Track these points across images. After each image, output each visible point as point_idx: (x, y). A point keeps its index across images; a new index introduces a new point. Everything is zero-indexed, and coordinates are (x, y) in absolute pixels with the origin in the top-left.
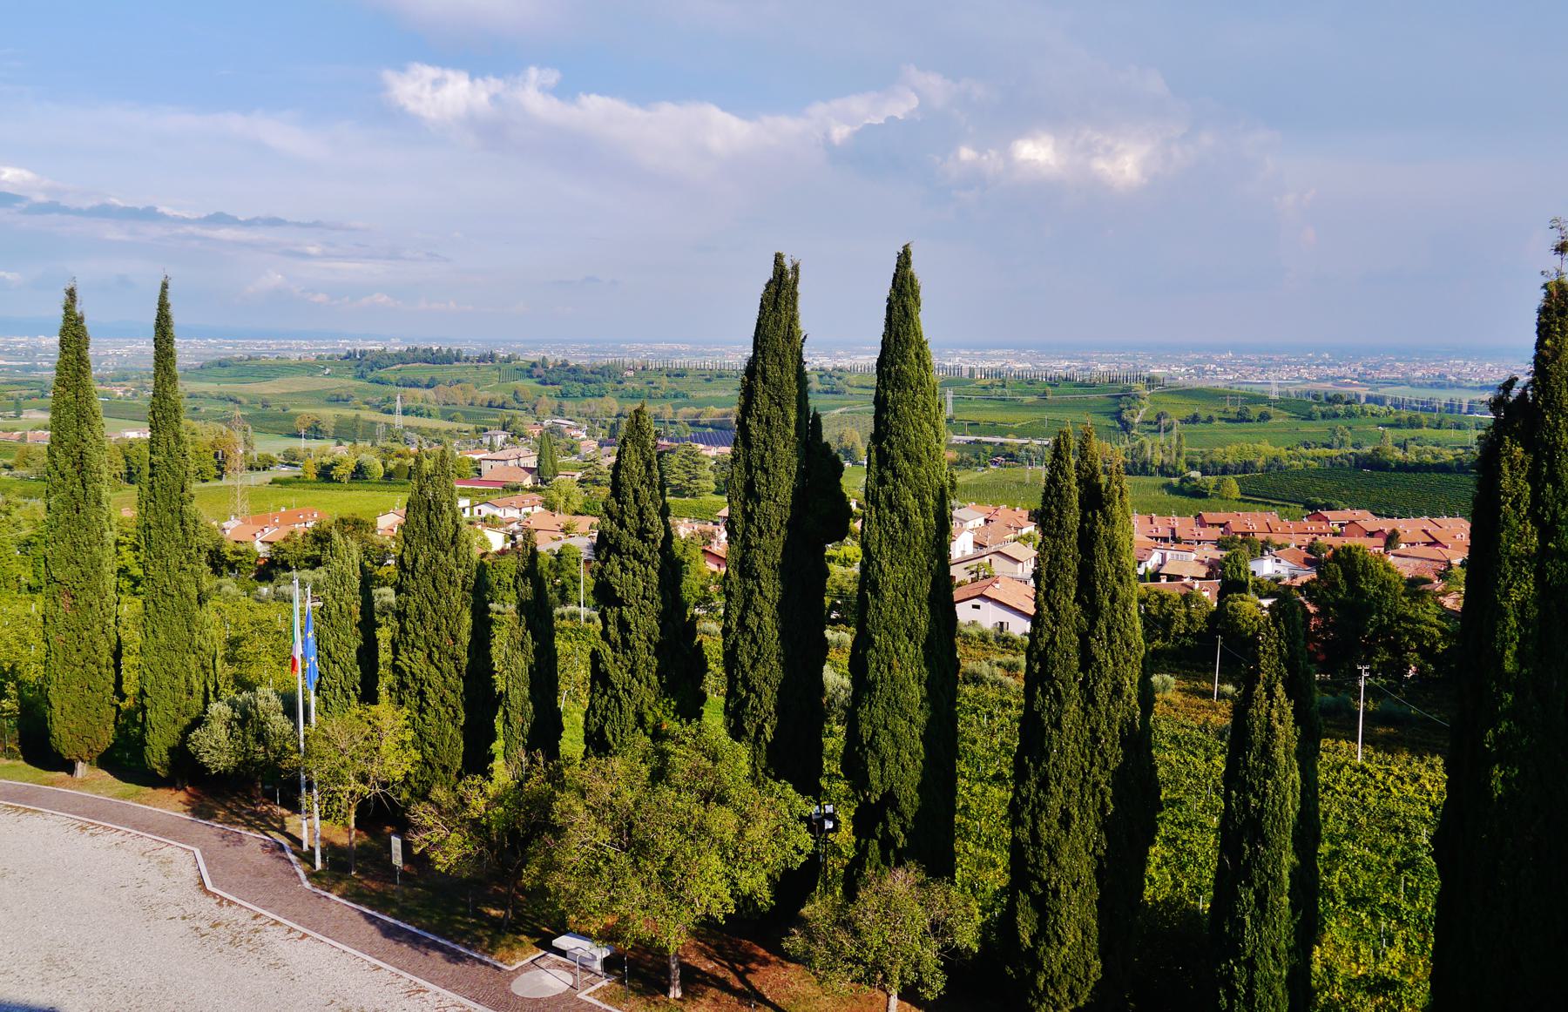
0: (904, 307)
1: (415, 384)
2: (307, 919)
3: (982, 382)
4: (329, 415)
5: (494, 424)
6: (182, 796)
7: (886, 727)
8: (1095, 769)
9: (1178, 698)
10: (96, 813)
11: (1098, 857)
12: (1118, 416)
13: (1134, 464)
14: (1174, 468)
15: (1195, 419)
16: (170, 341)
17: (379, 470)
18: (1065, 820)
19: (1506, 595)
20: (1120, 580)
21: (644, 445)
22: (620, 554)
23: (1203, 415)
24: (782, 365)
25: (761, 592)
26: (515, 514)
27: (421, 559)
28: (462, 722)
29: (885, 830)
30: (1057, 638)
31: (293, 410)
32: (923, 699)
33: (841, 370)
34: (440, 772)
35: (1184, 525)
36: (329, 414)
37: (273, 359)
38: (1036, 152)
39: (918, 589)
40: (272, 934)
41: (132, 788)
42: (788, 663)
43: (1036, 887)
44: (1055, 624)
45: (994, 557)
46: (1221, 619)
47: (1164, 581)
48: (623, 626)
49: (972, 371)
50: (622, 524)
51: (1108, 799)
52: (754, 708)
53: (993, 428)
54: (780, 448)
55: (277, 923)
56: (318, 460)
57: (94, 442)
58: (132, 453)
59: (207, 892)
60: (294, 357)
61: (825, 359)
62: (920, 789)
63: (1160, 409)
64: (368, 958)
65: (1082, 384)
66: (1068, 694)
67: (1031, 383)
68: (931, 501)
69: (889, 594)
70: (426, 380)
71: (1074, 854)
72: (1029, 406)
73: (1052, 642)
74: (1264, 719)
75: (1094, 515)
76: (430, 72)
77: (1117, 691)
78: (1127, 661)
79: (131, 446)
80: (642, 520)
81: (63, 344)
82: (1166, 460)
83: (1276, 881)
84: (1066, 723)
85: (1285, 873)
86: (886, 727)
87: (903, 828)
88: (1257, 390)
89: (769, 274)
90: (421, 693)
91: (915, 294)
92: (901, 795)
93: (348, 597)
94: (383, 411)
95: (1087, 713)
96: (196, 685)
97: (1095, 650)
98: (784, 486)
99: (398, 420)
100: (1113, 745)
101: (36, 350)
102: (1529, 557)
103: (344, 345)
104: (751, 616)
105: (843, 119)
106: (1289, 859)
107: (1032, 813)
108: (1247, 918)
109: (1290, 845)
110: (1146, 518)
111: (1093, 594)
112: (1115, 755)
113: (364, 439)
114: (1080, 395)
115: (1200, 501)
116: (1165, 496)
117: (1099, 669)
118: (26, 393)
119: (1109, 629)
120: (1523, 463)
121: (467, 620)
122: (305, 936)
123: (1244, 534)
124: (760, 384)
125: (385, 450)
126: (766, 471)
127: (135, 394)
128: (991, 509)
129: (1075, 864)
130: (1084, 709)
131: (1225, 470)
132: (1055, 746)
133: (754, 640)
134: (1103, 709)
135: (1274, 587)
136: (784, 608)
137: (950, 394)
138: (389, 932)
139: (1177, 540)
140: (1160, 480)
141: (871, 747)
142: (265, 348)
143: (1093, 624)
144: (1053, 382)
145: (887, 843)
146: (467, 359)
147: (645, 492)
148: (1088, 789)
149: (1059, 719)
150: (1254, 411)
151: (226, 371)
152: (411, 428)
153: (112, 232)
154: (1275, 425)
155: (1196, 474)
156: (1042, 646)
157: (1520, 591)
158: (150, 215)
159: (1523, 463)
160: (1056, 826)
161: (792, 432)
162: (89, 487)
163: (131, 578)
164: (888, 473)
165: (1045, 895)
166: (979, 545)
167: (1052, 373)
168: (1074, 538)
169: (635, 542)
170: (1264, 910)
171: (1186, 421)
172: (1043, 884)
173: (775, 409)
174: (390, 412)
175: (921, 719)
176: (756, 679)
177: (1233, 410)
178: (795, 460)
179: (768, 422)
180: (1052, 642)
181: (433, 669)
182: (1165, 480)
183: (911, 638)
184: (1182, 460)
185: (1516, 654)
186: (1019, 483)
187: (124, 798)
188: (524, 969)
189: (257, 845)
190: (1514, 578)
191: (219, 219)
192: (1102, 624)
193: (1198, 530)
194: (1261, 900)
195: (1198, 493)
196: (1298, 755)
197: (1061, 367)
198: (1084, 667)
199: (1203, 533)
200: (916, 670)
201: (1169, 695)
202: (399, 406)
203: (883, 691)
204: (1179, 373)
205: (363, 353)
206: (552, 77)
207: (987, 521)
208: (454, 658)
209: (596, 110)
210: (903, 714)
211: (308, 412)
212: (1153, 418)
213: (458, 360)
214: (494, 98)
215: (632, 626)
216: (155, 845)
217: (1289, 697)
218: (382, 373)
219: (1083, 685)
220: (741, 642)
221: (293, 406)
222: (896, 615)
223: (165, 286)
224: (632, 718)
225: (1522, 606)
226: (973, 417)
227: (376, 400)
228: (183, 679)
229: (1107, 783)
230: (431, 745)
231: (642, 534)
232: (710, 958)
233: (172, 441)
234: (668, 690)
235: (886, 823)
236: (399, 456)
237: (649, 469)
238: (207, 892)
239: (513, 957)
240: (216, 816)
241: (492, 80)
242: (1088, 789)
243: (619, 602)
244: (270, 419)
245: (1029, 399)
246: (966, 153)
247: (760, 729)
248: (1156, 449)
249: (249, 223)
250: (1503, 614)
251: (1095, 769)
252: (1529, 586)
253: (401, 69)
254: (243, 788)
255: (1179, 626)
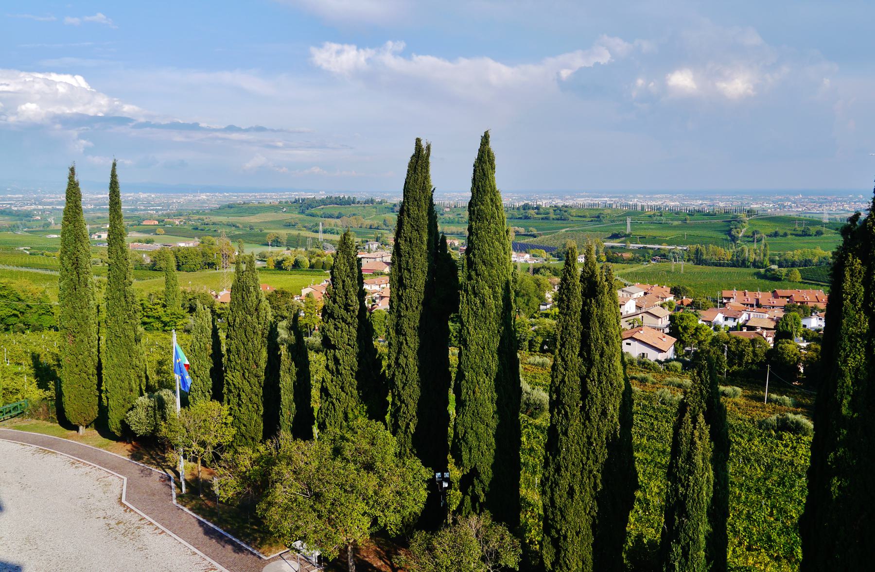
0: (483, 170)
1: (331, 217)
2: (167, 522)
3: (648, 213)
4: (283, 233)
5: (371, 238)
6: (129, 447)
7: (472, 429)
8: (590, 462)
9: (742, 401)
10: (84, 455)
11: (593, 517)
12: (729, 232)
13: (738, 261)
14: (762, 263)
15: (776, 234)
16: (118, 196)
17: (306, 262)
18: (571, 492)
19: (845, 362)
20: (607, 343)
21: (349, 254)
22: (335, 319)
23: (781, 232)
24: (419, 206)
25: (407, 344)
26: (377, 288)
27: (238, 320)
28: (261, 413)
29: (473, 491)
30: (566, 379)
31: (266, 231)
32: (495, 412)
33: (566, 207)
34: (250, 441)
35: (765, 297)
36: (283, 233)
37: (256, 203)
38: (682, 80)
39: (491, 345)
40: (148, 529)
41: (107, 441)
42: (424, 384)
43: (553, 533)
44: (565, 370)
45: (644, 315)
46: (774, 355)
47: (745, 331)
48: (336, 361)
49: (643, 207)
50: (335, 301)
51: (598, 481)
52: (404, 413)
53: (654, 240)
54: (417, 257)
55: (151, 523)
56: (275, 258)
57: (83, 252)
58: (180, 254)
59: (121, 503)
60: (267, 202)
61: (559, 201)
62: (493, 467)
63: (755, 229)
64: (192, 547)
65: (708, 214)
66: (572, 414)
67: (677, 213)
68: (500, 290)
69: (473, 348)
70: (336, 214)
71: (577, 514)
72: (676, 227)
73: (563, 381)
74: (689, 436)
75: (591, 301)
76: (335, 47)
77: (604, 413)
78: (611, 394)
79: (179, 251)
80: (346, 298)
81: (68, 198)
82: (757, 259)
83: (695, 541)
84: (571, 433)
85: (702, 537)
86: (472, 429)
87: (484, 491)
88: (816, 217)
89: (412, 151)
90: (239, 395)
91: (491, 162)
92: (481, 470)
93: (205, 340)
94: (313, 231)
95: (585, 426)
96: (134, 386)
97: (590, 386)
98: (420, 279)
99: (321, 236)
100: (601, 447)
101: (137, 200)
102: (861, 336)
103: (295, 195)
104: (401, 357)
105: (571, 64)
106: (704, 528)
107: (551, 487)
108: (677, 564)
109: (705, 519)
110: (741, 292)
111: (589, 351)
112: (603, 455)
113: (302, 246)
114: (707, 220)
115: (776, 283)
116: (755, 280)
117: (592, 399)
118: (130, 223)
119: (599, 374)
120: (860, 272)
121: (264, 354)
122: (163, 532)
123: (802, 303)
124: (406, 218)
125: (311, 252)
126: (409, 271)
127: (185, 223)
128: (648, 286)
129: (579, 518)
130: (584, 424)
131: (793, 265)
132: (564, 446)
133: (404, 373)
134: (595, 424)
135: (816, 334)
136: (422, 353)
137: (629, 220)
138: (208, 532)
139: (758, 305)
140: (753, 270)
141: (464, 441)
142: (253, 198)
143: (589, 371)
144: (691, 213)
145: (475, 498)
146: (359, 202)
147: (348, 281)
148: (585, 475)
149: (567, 430)
150: (813, 230)
151: (232, 210)
152: (327, 241)
153: (178, 137)
154: (826, 238)
155: (775, 267)
156: (557, 384)
157: (855, 360)
158: (195, 127)
159: (860, 272)
160: (565, 495)
161: (425, 247)
162: (81, 276)
163: (162, 322)
164: (473, 273)
165: (559, 538)
166: (639, 307)
167: (691, 208)
168: (578, 316)
169: (343, 312)
170: (687, 560)
171: (770, 236)
172: (558, 532)
173: (415, 233)
174: (317, 232)
175: (494, 424)
176: (405, 395)
177: (799, 229)
178: (427, 264)
179: (410, 241)
180: (563, 381)
181: (245, 382)
182: (757, 270)
183: (487, 375)
184: (767, 259)
185: (849, 403)
186: (667, 271)
187: (100, 447)
188: (274, 559)
189: (157, 477)
190: (851, 351)
191: (231, 129)
192: (594, 371)
193: (772, 299)
194: (685, 554)
195: (776, 278)
196: (712, 461)
197: (696, 204)
198: (583, 399)
199: (776, 302)
200: (490, 394)
201: (737, 399)
202: (321, 228)
203: (470, 406)
204: (769, 208)
205: (303, 200)
206: (401, 46)
207: (645, 294)
208: (257, 376)
209: (426, 63)
210: (483, 422)
211: (274, 232)
212: (750, 234)
213: (354, 203)
214: (368, 60)
215: (341, 362)
216: (106, 475)
217: (707, 423)
218: (313, 211)
219: (583, 408)
220: (397, 373)
221: (266, 229)
222: (477, 360)
223: (114, 165)
224: (341, 415)
225: (857, 370)
226: (642, 233)
227: (310, 225)
228: (127, 383)
229: (598, 471)
230: (245, 425)
231: (347, 307)
232: (380, 558)
233: (119, 251)
234: (364, 398)
235: (474, 487)
236: (318, 256)
237: (352, 269)
238: (121, 503)
239: (270, 551)
240: (142, 459)
241: (368, 50)
242: (585, 475)
243: (334, 347)
244: (254, 236)
245: (676, 223)
246: (640, 82)
247: (408, 425)
248: (751, 252)
249: (247, 131)
250: (842, 375)
251: (590, 462)
252: (861, 357)
253: (320, 46)
254: (149, 446)
255: (748, 358)
